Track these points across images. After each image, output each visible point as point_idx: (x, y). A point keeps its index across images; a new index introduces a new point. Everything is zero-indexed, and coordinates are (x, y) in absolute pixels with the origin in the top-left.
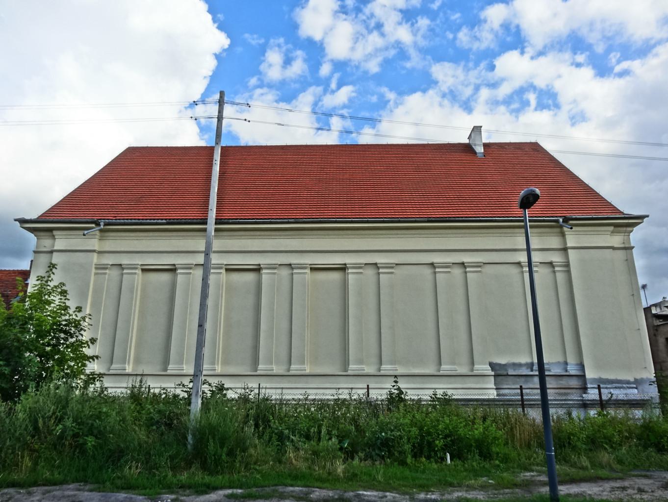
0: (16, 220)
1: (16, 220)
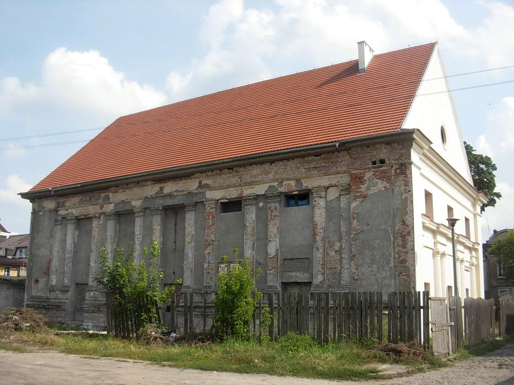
0: (18, 194)
1: (18, 194)
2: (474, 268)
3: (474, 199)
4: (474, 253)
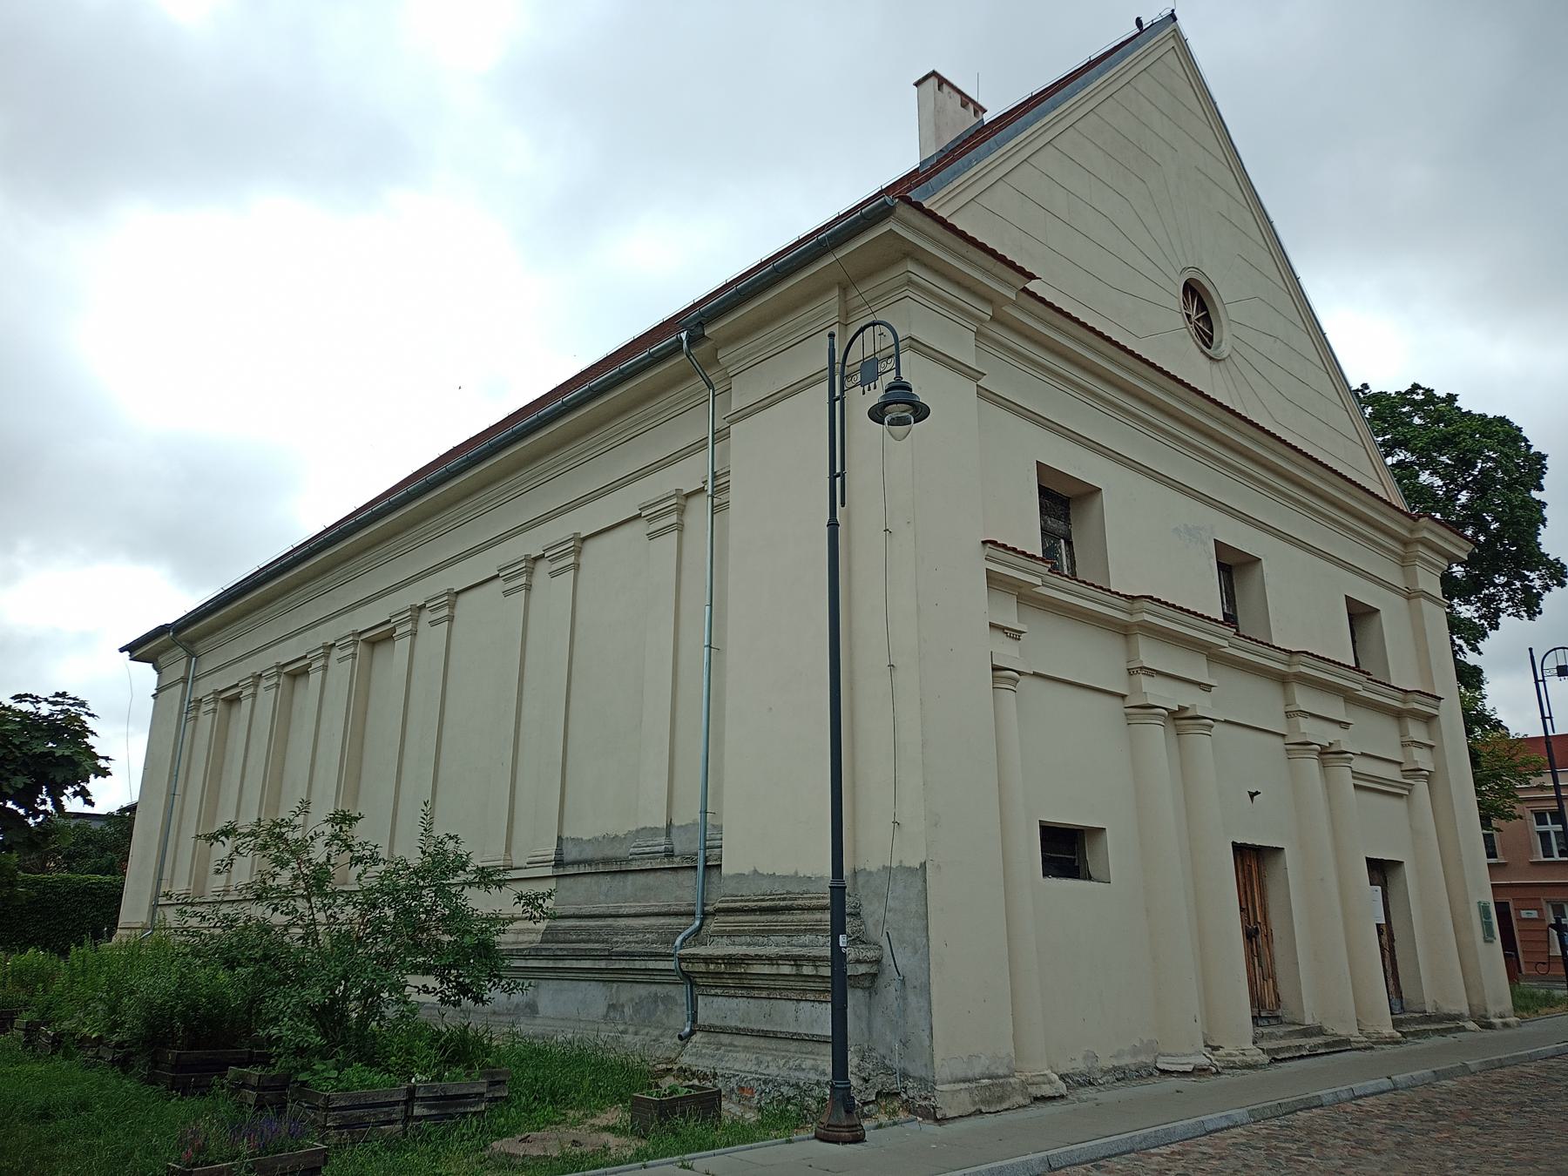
0: (122, 650)
1: (122, 650)
2: (1421, 786)
3: (1406, 543)
4: (1416, 731)
